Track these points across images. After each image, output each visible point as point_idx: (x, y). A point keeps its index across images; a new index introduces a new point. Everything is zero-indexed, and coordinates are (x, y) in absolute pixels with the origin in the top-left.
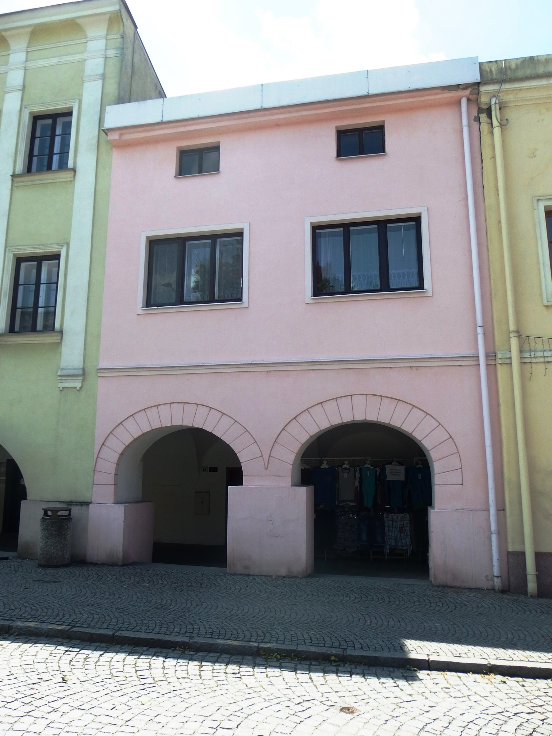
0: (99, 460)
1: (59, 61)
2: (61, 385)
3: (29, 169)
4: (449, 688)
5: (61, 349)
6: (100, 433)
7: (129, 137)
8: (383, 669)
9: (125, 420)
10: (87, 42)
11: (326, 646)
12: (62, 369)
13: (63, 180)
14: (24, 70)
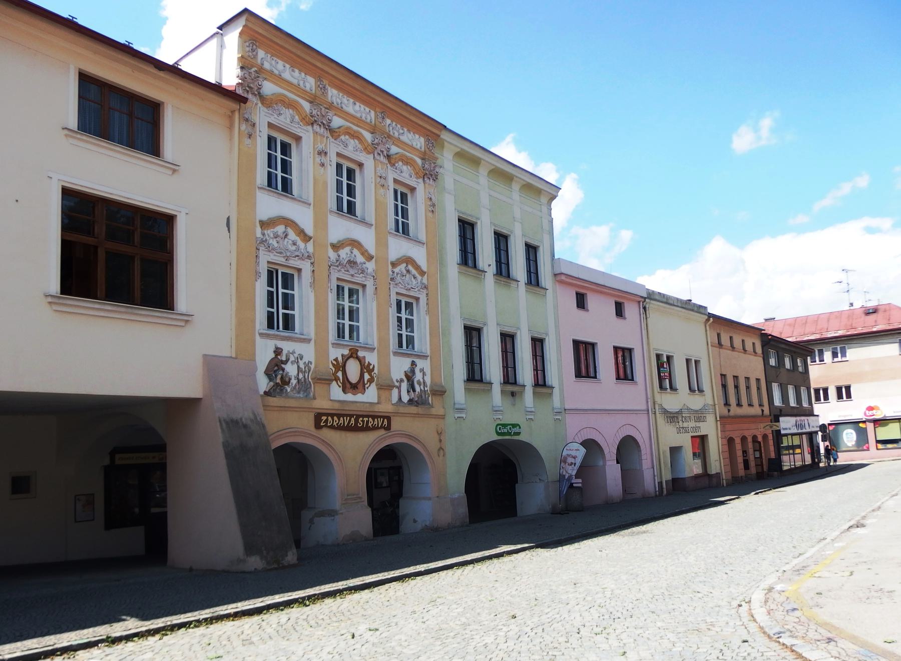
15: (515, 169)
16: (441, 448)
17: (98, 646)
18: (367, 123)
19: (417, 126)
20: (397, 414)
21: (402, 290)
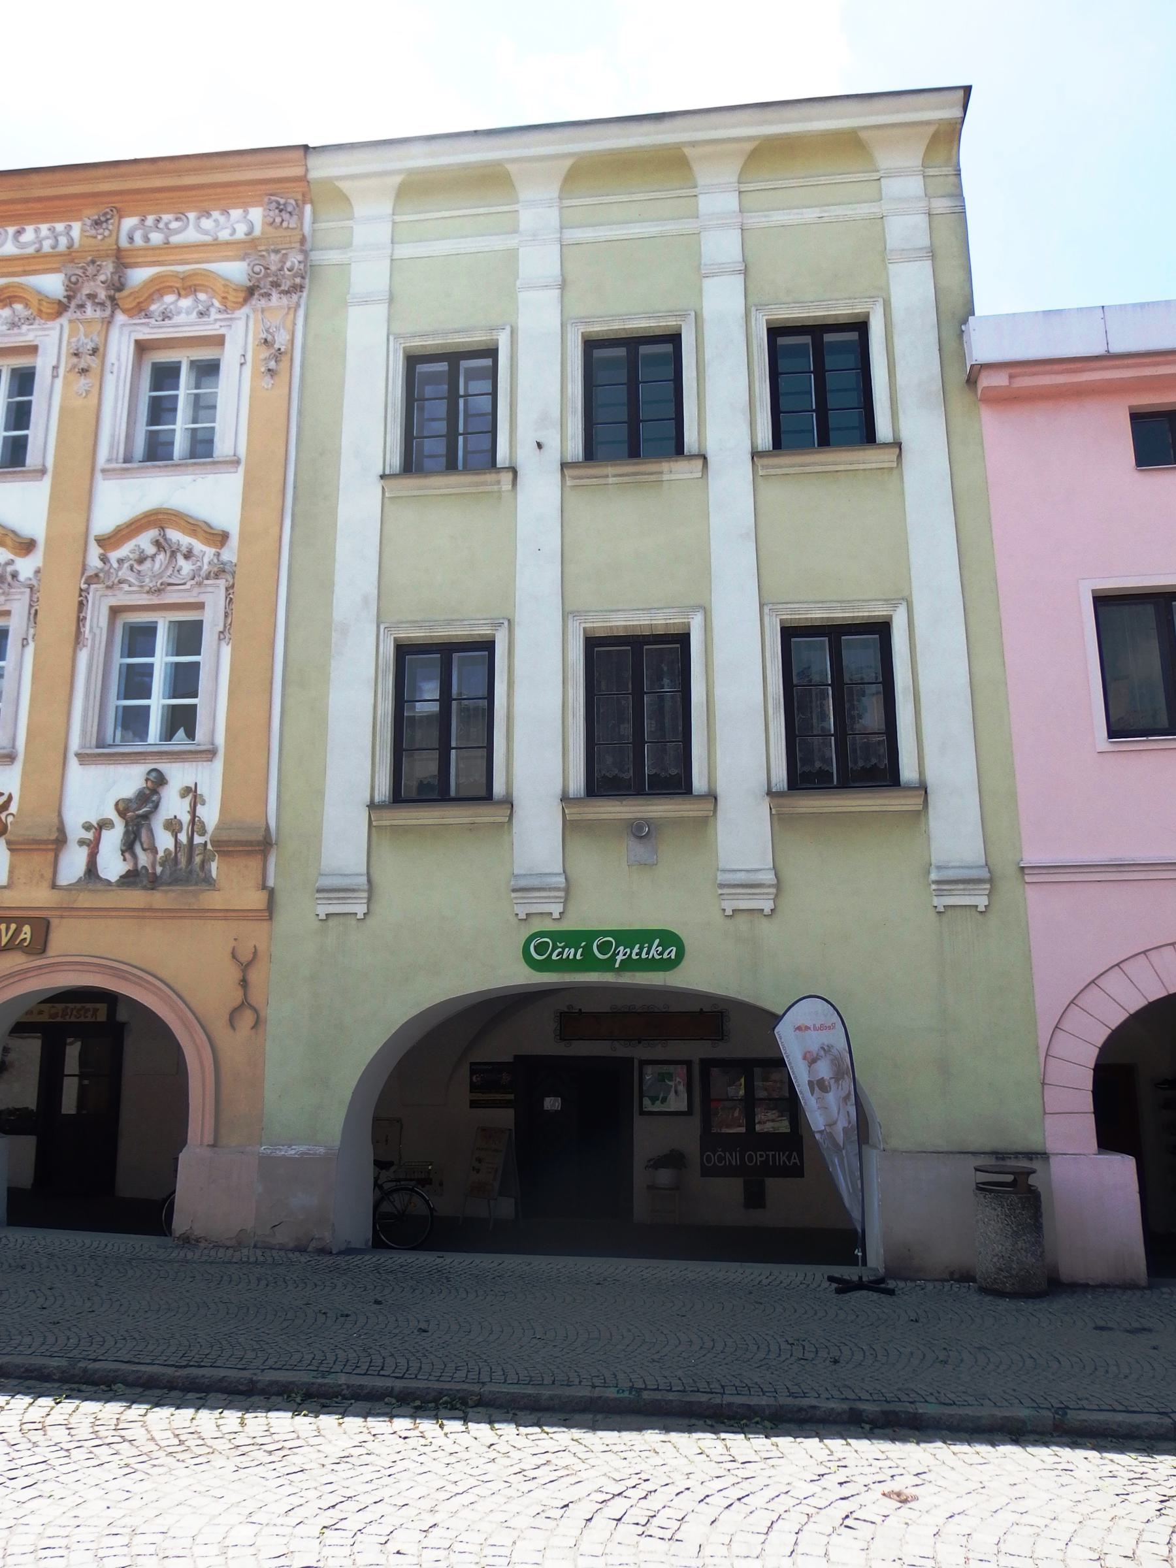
0: (1051, 1060)
1: (821, 215)
2: (941, 902)
3: (591, 453)
4: (1071, 1471)
5: (927, 824)
6: (1047, 1005)
7: (1026, 382)
8: (705, 1422)
9: (1102, 974)
10: (879, 179)
11: (673, 1389)
12: (939, 868)
13: (874, 466)
14: (740, 230)
15: (667, 125)
16: (245, 1004)
17: (415, 1421)
18: (46, 256)
19: (219, 190)
20: (68, 911)
21: (137, 596)
